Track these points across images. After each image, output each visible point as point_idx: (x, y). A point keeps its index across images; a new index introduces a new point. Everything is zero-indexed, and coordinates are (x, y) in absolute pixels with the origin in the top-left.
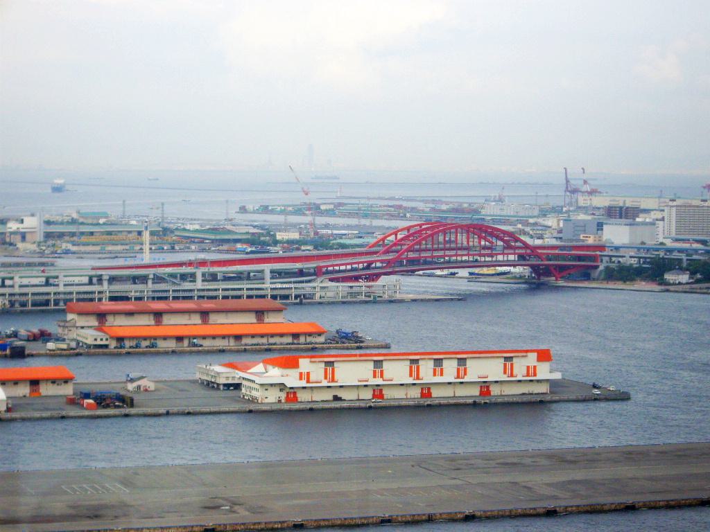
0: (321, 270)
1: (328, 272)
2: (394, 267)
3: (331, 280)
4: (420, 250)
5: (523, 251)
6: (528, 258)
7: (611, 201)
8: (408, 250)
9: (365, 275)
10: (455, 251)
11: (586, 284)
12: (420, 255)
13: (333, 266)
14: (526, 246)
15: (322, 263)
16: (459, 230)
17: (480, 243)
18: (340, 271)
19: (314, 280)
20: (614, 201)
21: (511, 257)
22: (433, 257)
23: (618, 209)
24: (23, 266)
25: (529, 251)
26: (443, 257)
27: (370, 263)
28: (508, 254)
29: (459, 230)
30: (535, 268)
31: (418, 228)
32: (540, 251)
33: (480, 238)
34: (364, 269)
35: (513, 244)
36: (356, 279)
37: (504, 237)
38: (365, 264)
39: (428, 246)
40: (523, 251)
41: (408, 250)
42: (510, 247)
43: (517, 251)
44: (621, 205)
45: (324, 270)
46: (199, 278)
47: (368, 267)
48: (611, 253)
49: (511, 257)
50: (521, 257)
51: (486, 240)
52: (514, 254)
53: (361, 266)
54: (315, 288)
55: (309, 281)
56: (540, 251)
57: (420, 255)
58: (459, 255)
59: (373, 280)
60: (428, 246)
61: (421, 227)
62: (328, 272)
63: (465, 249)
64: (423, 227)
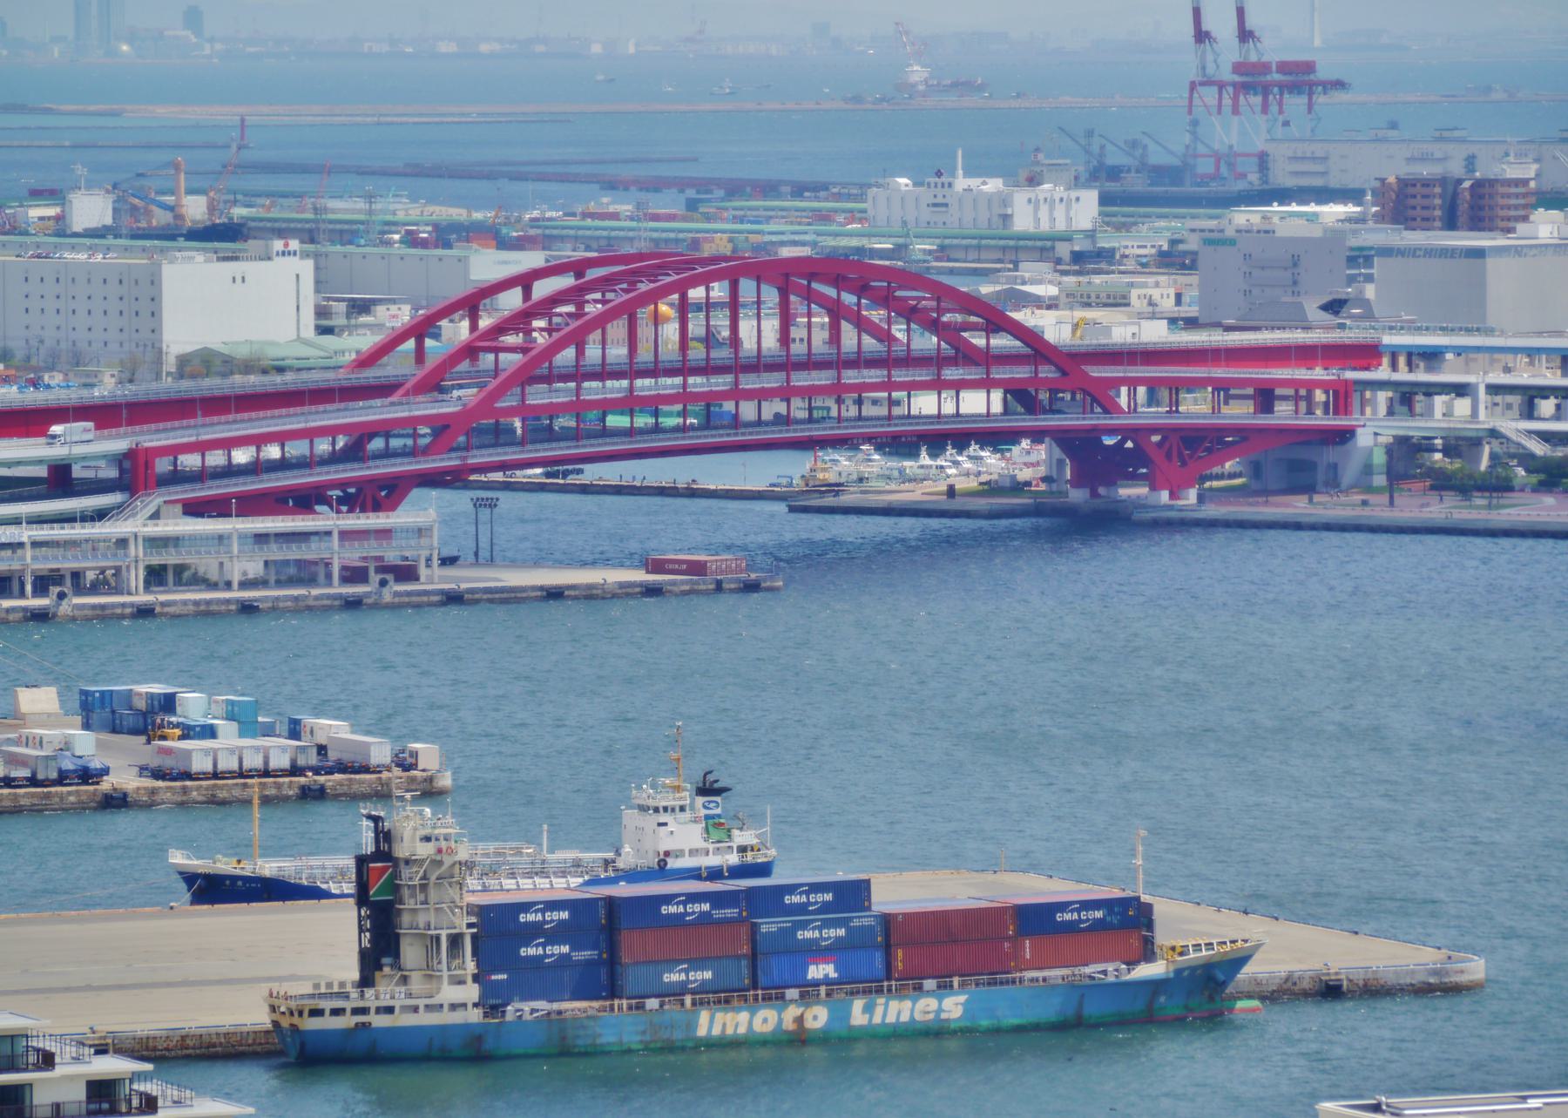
0: (149, 465)
1: (177, 477)
2: (467, 448)
3: (194, 509)
4: (579, 374)
5: (1021, 373)
6: (1044, 396)
7: (1411, 160)
8: (526, 377)
9: (342, 484)
10: (729, 378)
11: (1298, 506)
12: (685, 385)
13: (202, 447)
14: (1037, 348)
15: (152, 438)
16: (747, 287)
17: (835, 337)
18: (230, 471)
19: (120, 508)
20: (1423, 159)
21: (974, 403)
22: (578, 407)
23: (1438, 190)
24: (173, 740)
25: (1047, 372)
26: (630, 404)
27: (364, 434)
28: (959, 386)
29: (747, 287)
30: (1079, 446)
31: (512, 300)
32: (1096, 372)
33: (836, 312)
34: (334, 458)
35: (979, 341)
36: (305, 500)
37: (940, 311)
38: (341, 442)
39: (714, 354)
40: (1021, 373)
41: (526, 377)
42: (967, 355)
43: (999, 373)
44: (1456, 168)
45: (163, 465)
46: (136, 577)
47: (354, 452)
48: (1403, 375)
49: (974, 403)
50: (1020, 395)
51: (862, 325)
52: (987, 384)
53: (323, 446)
54: (122, 543)
55: (100, 515)
56: (1096, 372)
57: (685, 385)
58: (750, 395)
59: (377, 507)
60: (714, 354)
61: (527, 294)
62: (177, 477)
63: (772, 367)
64: (593, 274)
